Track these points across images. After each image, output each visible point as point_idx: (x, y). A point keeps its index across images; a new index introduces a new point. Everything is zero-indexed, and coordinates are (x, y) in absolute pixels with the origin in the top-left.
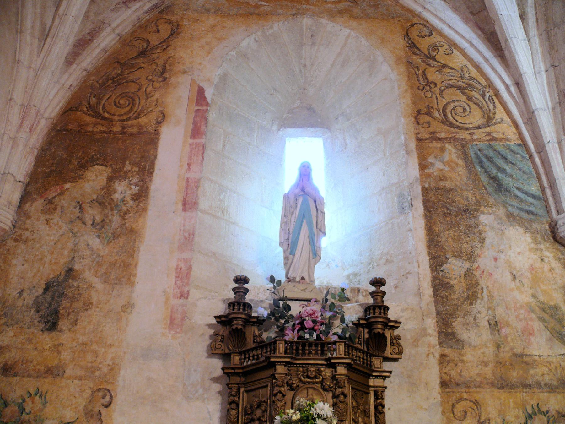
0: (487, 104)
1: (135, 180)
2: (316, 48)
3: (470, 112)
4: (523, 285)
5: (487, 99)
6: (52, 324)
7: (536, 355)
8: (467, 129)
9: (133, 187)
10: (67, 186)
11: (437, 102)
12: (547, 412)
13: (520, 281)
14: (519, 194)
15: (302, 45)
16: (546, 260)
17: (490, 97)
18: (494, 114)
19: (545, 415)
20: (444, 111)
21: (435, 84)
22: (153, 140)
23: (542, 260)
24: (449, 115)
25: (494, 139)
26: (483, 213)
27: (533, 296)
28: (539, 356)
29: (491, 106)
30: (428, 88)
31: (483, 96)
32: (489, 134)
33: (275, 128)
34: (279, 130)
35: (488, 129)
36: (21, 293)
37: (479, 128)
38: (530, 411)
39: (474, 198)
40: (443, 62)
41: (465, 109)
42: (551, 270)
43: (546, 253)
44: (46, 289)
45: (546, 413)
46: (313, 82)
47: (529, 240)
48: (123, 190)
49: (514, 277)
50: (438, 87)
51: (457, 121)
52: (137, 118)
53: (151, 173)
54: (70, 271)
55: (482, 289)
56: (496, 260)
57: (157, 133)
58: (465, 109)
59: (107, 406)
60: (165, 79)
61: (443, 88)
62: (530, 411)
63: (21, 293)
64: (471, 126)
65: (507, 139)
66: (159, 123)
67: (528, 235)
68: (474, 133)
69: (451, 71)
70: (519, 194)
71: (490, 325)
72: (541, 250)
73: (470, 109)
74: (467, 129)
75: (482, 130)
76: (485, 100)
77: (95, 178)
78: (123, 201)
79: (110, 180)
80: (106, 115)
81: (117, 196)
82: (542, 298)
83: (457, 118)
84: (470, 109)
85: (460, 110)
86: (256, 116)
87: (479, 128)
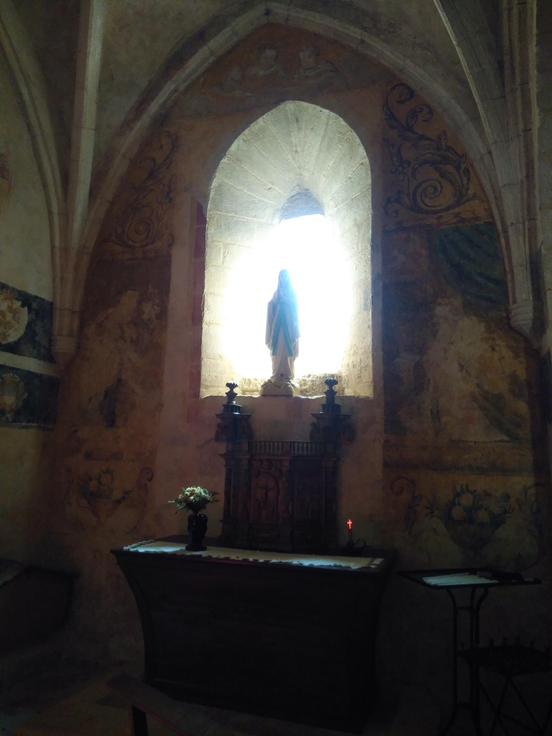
0: (461, 177)
1: (157, 301)
2: (303, 133)
3: (441, 192)
4: (470, 375)
5: (461, 172)
6: (111, 423)
7: (471, 442)
8: (435, 212)
9: (156, 307)
10: (110, 311)
11: (408, 185)
12: (475, 491)
13: (468, 372)
14: (479, 279)
15: (291, 132)
16: (497, 349)
17: (465, 168)
18: (467, 189)
19: (472, 494)
20: (414, 194)
21: (409, 163)
22: (167, 263)
23: (493, 349)
24: (419, 199)
25: (463, 220)
26: (440, 304)
27: (478, 385)
28: (475, 442)
29: (465, 181)
30: (401, 169)
31: (458, 168)
32: (457, 215)
33: (276, 220)
34: (280, 222)
35: (457, 210)
36: (90, 399)
37: (448, 209)
38: (458, 490)
39: (432, 290)
40: (420, 133)
41: (435, 189)
42: (502, 358)
43: (499, 342)
44: (106, 396)
45: (473, 493)
46: (306, 167)
47: (483, 329)
48: (149, 310)
49: (462, 367)
50: (412, 165)
51: (426, 205)
52: (153, 242)
53: (167, 292)
54: (119, 380)
55: (429, 380)
56: (446, 351)
57: (169, 255)
58: (435, 189)
59: (150, 480)
60: (171, 200)
61: (416, 167)
62: (458, 490)
63: (90, 399)
64: (439, 208)
65: (477, 219)
66: (170, 245)
67: (482, 324)
68: (441, 217)
69: (428, 142)
70: (479, 279)
71: (432, 413)
72: (494, 339)
73: (442, 187)
74: (435, 212)
75: (451, 211)
76: (459, 174)
77: (129, 300)
78: (150, 320)
79: (140, 302)
80: (130, 243)
81: (146, 317)
82: (486, 387)
83: (427, 201)
84: (442, 187)
85: (431, 190)
86: (255, 217)
87: (448, 209)
